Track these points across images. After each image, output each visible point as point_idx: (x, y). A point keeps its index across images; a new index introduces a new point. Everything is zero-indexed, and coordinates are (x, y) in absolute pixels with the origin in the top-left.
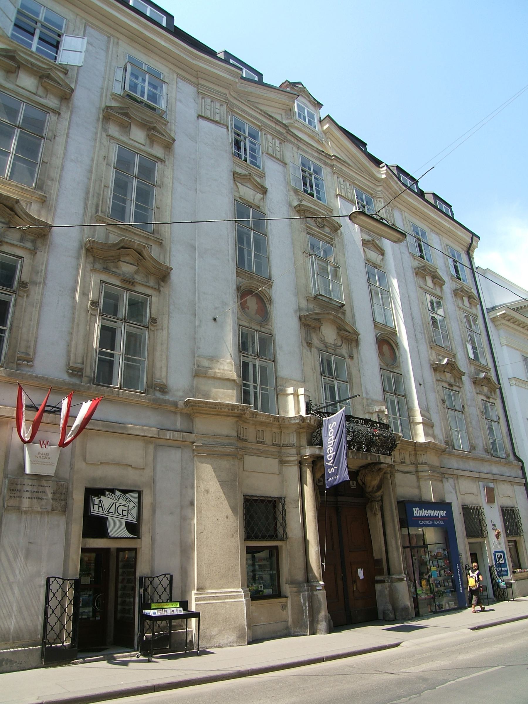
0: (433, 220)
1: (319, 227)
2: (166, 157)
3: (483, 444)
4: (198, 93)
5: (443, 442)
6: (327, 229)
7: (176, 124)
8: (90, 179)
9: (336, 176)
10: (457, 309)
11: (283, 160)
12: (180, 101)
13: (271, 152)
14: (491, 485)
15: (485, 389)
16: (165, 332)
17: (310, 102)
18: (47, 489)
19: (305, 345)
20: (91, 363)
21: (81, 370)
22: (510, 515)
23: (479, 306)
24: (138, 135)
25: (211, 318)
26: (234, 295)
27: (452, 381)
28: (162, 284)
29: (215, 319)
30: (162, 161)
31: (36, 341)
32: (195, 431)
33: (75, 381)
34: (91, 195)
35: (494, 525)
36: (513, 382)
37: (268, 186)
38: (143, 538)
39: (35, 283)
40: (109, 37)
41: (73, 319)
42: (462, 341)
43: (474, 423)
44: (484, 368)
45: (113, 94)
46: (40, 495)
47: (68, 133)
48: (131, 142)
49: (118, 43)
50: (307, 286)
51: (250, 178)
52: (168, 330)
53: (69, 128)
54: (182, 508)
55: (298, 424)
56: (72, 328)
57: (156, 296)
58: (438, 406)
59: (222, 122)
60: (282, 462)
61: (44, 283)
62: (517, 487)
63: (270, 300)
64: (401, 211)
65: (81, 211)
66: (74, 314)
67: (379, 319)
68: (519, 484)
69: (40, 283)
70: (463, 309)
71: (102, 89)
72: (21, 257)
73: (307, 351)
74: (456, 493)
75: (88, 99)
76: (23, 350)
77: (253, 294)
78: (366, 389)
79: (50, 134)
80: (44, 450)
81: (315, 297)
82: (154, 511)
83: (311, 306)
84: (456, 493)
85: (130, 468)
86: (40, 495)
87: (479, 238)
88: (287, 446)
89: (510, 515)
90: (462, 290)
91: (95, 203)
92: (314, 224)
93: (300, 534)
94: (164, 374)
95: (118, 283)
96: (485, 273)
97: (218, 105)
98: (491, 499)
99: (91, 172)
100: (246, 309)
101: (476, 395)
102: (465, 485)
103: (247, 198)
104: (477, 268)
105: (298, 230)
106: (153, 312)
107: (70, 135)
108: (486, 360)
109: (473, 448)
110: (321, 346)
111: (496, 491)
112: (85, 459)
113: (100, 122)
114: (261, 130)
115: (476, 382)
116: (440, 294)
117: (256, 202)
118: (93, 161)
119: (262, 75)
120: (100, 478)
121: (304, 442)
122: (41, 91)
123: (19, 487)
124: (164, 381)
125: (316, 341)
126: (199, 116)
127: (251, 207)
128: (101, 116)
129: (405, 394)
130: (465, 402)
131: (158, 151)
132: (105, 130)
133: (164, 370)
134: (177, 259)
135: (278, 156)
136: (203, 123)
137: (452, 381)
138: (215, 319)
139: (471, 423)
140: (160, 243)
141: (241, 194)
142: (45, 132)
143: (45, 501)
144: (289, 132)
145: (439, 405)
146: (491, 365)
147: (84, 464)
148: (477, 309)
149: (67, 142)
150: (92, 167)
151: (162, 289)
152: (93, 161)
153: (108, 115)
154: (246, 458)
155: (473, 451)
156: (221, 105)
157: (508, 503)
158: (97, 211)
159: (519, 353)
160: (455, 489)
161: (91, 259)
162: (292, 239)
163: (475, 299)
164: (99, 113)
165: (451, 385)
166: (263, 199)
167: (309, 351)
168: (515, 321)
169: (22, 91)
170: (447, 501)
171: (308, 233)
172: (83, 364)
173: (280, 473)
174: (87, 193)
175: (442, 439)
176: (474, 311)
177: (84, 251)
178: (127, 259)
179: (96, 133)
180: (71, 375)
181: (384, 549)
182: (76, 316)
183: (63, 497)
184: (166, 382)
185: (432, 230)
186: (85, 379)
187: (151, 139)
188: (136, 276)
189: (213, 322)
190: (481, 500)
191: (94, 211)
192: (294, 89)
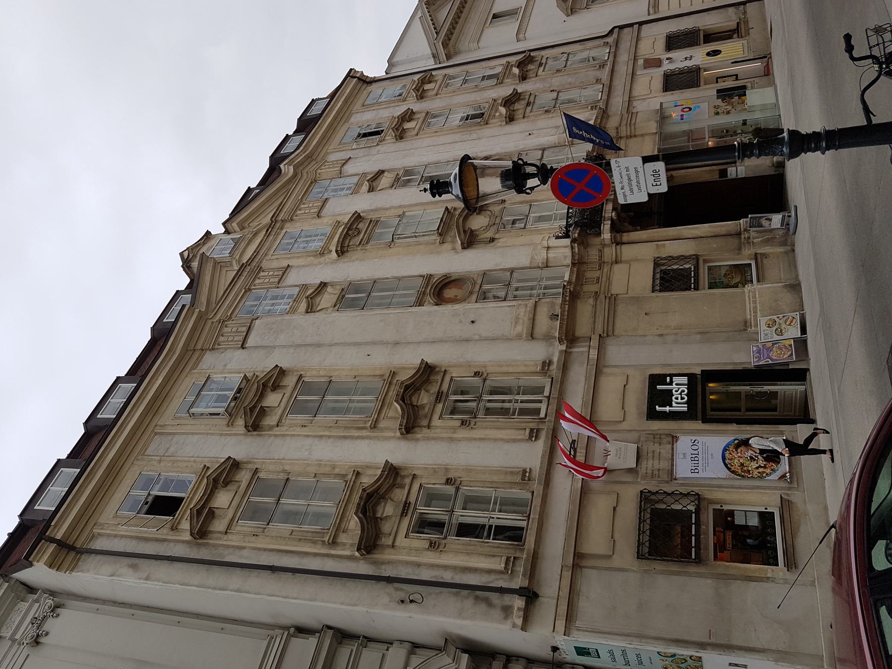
0: (335, 118)
1: (359, 233)
4: (213, 349)
6: (361, 226)
9: (295, 218)
12: (226, 365)
13: (277, 280)
14: (641, 62)
15: (531, 67)
17: (204, 244)
18: (651, 450)
19: (492, 244)
20: (525, 422)
22: (674, 42)
23: (434, 73)
27: (524, 103)
29: (473, 322)
32: (589, 335)
33: (543, 435)
35: (686, 59)
36: (521, 36)
38: (249, 440)
40: (156, 434)
42: (514, 441)
43: (570, 80)
44: (508, 66)
45: (228, 425)
46: (656, 455)
49: (161, 426)
55: (579, 245)
62: (643, 34)
64: (327, 154)
65: (367, 441)
68: (639, 30)
70: (438, 90)
72: (421, 485)
75: (235, 445)
77: (440, 290)
80: (613, 453)
81: (440, 235)
82: (670, 365)
83: (449, 239)
86: (656, 455)
87: (351, 70)
88: (601, 257)
89: (674, 42)
90: (417, 89)
92: (357, 238)
93: (692, 243)
95: (440, 406)
96: (391, 63)
97: (226, 330)
98: (658, 63)
99: (321, 437)
102: (640, 88)
104: (387, 73)
108: (497, 67)
109: (598, 81)
110: (493, 229)
111: (647, 57)
115: (523, 78)
116: (424, 115)
117: (338, 292)
119: (178, 291)
121: (597, 240)
122: (232, 487)
123: (649, 471)
125: (489, 234)
127: (343, 296)
128: (255, 433)
129: (540, 149)
132: (271, 428)
135: (281, 273)
136: (250, 342)
137: (524, 103)
139: (570, 84)
140: (393, 374)
146: (503, 61)
147: (615, 556)
148: (437, 75)
150: (316, 436)
153: (255, 427)
154: (613, 292)
155: (603, 81)
157: (661, 43)
159: (486, 30)
161: (416, 429)
163: (426, 77)
164: (252, 435)
165: (528, 104)
166: (333, 284)
168: (450, 33)
169: (235, 503)
173: (628, 262)
176: (440, 78)
177: (410, 435)
179: (276, 436)
180: (537, 438)
181: (709, 168)
186: (541, 426)
187: (276, 387)
190: (657, 74)
192: (191, 260)
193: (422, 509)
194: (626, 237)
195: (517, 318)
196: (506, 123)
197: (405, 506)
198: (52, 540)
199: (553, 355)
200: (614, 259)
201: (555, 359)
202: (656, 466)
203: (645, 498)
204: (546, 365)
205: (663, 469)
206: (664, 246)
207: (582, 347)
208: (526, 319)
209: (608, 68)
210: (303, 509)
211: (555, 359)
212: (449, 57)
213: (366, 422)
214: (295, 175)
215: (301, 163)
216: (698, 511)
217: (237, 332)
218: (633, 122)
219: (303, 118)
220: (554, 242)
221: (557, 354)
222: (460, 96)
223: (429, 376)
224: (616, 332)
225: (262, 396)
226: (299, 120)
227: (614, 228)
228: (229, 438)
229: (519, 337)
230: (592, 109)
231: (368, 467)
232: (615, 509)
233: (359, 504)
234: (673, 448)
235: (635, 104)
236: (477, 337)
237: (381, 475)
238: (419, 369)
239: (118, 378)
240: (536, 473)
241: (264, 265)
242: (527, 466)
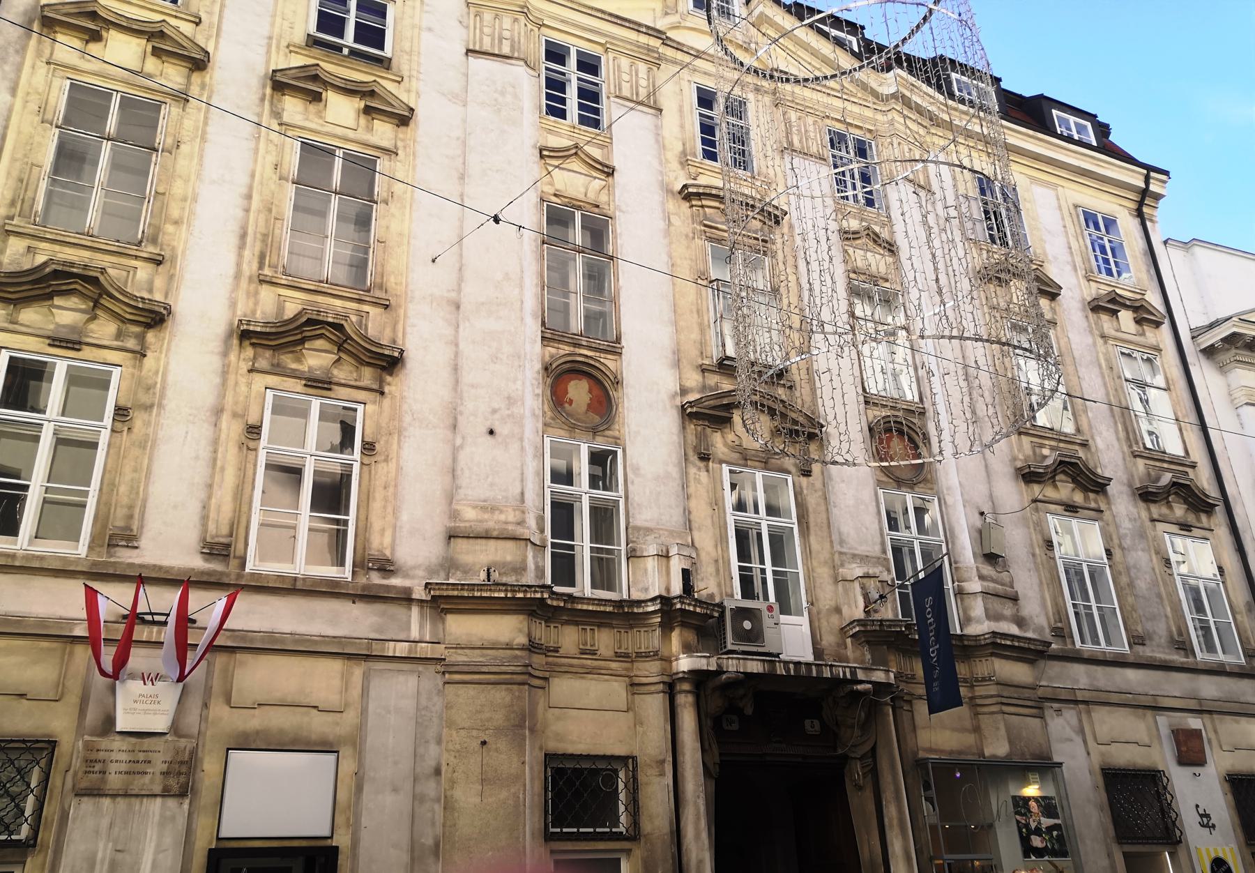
2: (400, 144)
3: (1170, 632)
5: (1047, 631)
7: (421, 76)
8: (247, 210)
10: (1100, 341)
11: (655, 102)
12: (430, 29)
13: (626, 92)
14: (1194, 723)
16: (392, 465)
19: (693, 458)
21: (228, 546)
23: (1166, 327)
24: (341, 111)
25: (484, 430)
26: (535, 382)
28: (389, 379)
29: (491, 432)
30: (391, 152)
31: (144, 506)
34: (249, 239)
37: (616, 162)
39: (148, 408)
41: (215, 460)
47: (204, 132)
48: (329, 128)
50: (702, 344)
51: (576, 154)
52: (398, 461)
53: (206, 123)
54: (416, 779)
56: (212, 476)
57: (375, 402)
58: (1034, 555)
59: (516, 55)
60: (634, 686)
61: (160, 405)
63: (617, 382)
66: (215, 451)
67: (441, 626)
69: (152, 406)
71: (270, 38)
73: (699, 469)
74: (1085, 742)
76: (120, 523)
78: (840, 533)
79: (169, 141)
82: (359, 789)
84: (1085, 742)
85: (315, 711)
91: (257, 253)
94: (387, 540)
97: (507, 22)
99: (249, 197)
100: (567, 405)
101: (1148, 524)
102: (1109, 722)
103: (572, 192)
105: (687, 236)
106: (368, 431)
107: (209, 136)
112: (228, 701)
113: (267, 103)
114: (606, 50)
117: (591, 197)
118: (253, 176)
120: (258, 732)
123: (101, 755)
124: (388, 553)
126: (469, 52)
130: (1116, 541)
131: (383, 132)
133: (388, 534)
134: (420, 335)
138: (491, 432)
139: (1131, 585)
141: (558, 186)
142: (159, 138)
143: (148, 777)
144: (666, 41)
145: (1037, 551)
146: (1198, 455)
147: (227, 708)
149: (201, 150)
150: (251, 188)
151: (387, 389)
152: (253, 176)
156: (516, 20)
158: (261, 266)
160: (1082, 732)
162: (670, 257)
164: (264, 87)
166: (609, 188)
167: (703, 469)
170: (1056, 759)
171: (710, 239)
172: (231, 536)
174: (243, 236)
175: (1045, 624)
178: (320, 343)
182: (219, 455)
183: (184, 769)
184: (392, 554)
185: (1034, 180)
188: (335, 372)
189: (489, 437)
191: (255, 265)
193: (60, 370)
194: (685, 702)
195: (493, 509)
196: (1020, 469)
197: (74, 343)
198: (1147, 179)
199: (406, 576)
200: (637, 680)
201: (395, 581)
202: (113, 768)
203: (44, 748)
204: (386, 567)
205: (104, 781)
206: (662, 774)
207: (421, 627)
208: (491, 524)
209: (1178, 658)
210: (572, 287)
211: (395, 581)
212: (1209, 352)
213: (273, 267)
214: (884, 99)
215: (907, 102)
216: (618, 837)
217: (501, 39)
218: (1005, 709)
219: (1045, 104)
220: (677, 565)
221: (405, 583)
222: (1099, 381)
223: (369, 364)
224: (449, 688)
225: (349, 90)
226: (1041, 97)
227: (699, 678)
228: (263, 50)
229: (454, 515)
230: (1054, 629)
231: (171, 277)
232: (22, 696)
233: (72, 264)
234: (156, 796)
235: (1070, 714)
236: (458, 442)
237: (135, 298)
238: (1094, 474)
239: (1095, 116)
240: (126, 556)
241: (667, 70)
242: (144, 542)
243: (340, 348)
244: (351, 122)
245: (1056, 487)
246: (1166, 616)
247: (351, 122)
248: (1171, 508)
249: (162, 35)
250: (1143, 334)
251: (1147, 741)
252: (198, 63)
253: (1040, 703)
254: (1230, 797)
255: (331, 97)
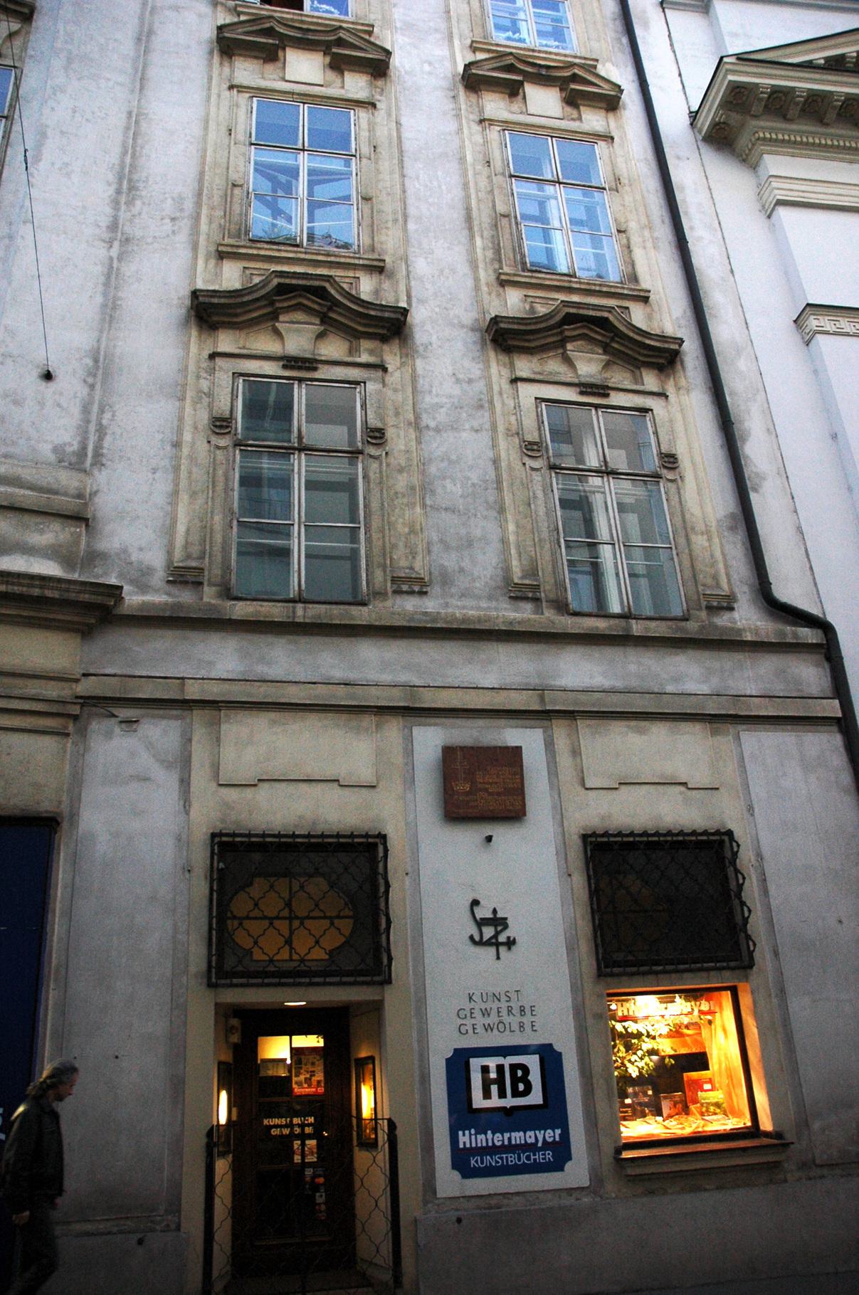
58: (177, 445)
160: (184, 763)
235: (161, 732)
243: (324, 319)
244: (558, 113)
245: (277, 333)
246: (504, 541)
247: (558, 113)
248: (568, 361)
249: (340, 42)
250: (580, 119)
251: (367, 775)
252: (378, 67)
253: (79, 711)
254: (579, 880)
255: (531, 90)
